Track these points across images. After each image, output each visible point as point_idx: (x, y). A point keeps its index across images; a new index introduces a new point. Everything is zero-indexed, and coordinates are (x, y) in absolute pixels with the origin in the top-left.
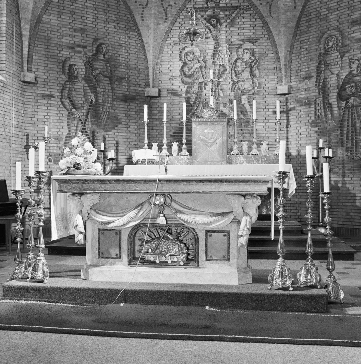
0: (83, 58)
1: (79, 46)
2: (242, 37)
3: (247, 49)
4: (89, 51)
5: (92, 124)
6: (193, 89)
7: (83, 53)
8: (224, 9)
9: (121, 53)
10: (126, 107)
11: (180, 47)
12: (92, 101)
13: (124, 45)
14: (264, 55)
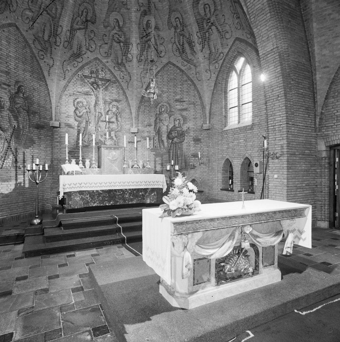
0: (7, 94)
1: (5, 84)
2: (112, 98)
3: (115, 105)
4: (12, 89)
5: (15, 143)
6: (82, 125)
7: (8, 90)
8: (101, 80)
9: (35, 95)
10: (38, 132)
11: (74, 97)
12: (15, 126)
13: (37, 90)
14: (123, 110)
